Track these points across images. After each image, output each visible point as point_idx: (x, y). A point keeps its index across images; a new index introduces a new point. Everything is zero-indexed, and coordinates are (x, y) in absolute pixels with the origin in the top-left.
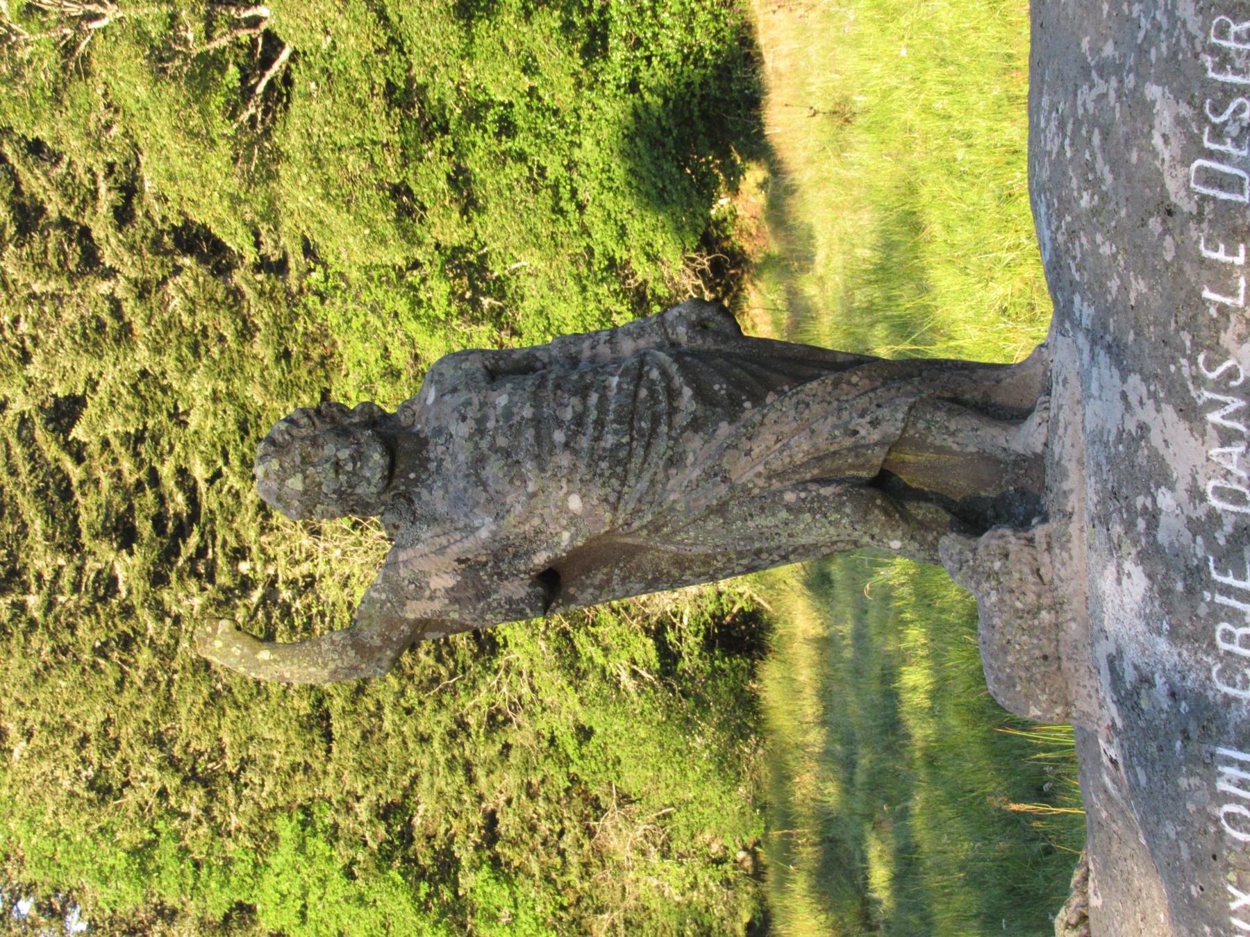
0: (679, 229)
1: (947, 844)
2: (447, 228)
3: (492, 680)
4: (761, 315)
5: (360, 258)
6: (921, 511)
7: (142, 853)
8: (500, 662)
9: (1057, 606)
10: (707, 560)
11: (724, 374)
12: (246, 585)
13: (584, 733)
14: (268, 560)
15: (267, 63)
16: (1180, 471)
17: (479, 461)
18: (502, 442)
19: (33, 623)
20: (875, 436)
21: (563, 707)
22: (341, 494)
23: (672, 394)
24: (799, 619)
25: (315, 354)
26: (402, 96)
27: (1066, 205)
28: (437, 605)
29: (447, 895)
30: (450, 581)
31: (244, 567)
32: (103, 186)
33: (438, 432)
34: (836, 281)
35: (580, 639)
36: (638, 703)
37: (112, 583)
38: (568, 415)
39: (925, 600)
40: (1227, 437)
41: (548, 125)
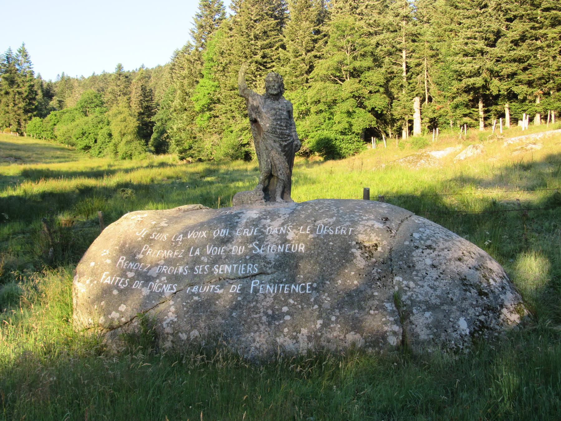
0: (313, 147)
1: (213, 190)
2: (313, 109)
3: (240, 117)
4: (297, 160)
5: (308, 96)
6: (267, 182)
7: (212, 60)
8: (243, 118)
9: (251, 203)
10: (259, 147)
11: (289, 149)
12: (256, 77)
13: (232, 132)
14: (259, 80)
15: (340, 80)
16: (273, 223)
17: (275, 109)
18: (278, 113)
19: (249, 42)
20: (279, 174)
21: (236, 128)
22: (269, 87)
23: (286, 141)
24: (250, 166)
25: (293, 88)
26: (335, 102)
27: (316, 205)
28: (251, 102)
29: (205, 110)
30: (255, 105)
31: (258, 76)
32: (320, 53)
33: (279, 103)
34: (305, 172)
35: (247, 131)
36: (237, 140)
37: (256, 55)
38: (282, 124)
39: (253, 185)
40: (279, 231)
41: (330, 125)
